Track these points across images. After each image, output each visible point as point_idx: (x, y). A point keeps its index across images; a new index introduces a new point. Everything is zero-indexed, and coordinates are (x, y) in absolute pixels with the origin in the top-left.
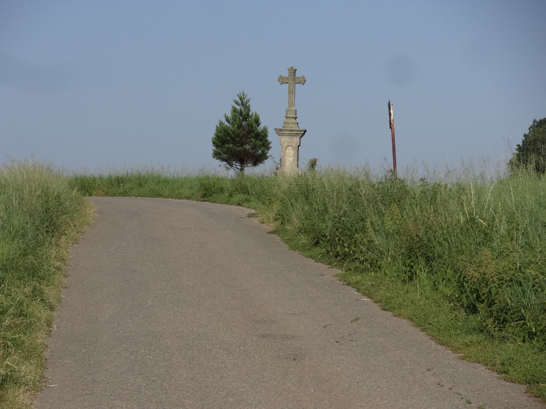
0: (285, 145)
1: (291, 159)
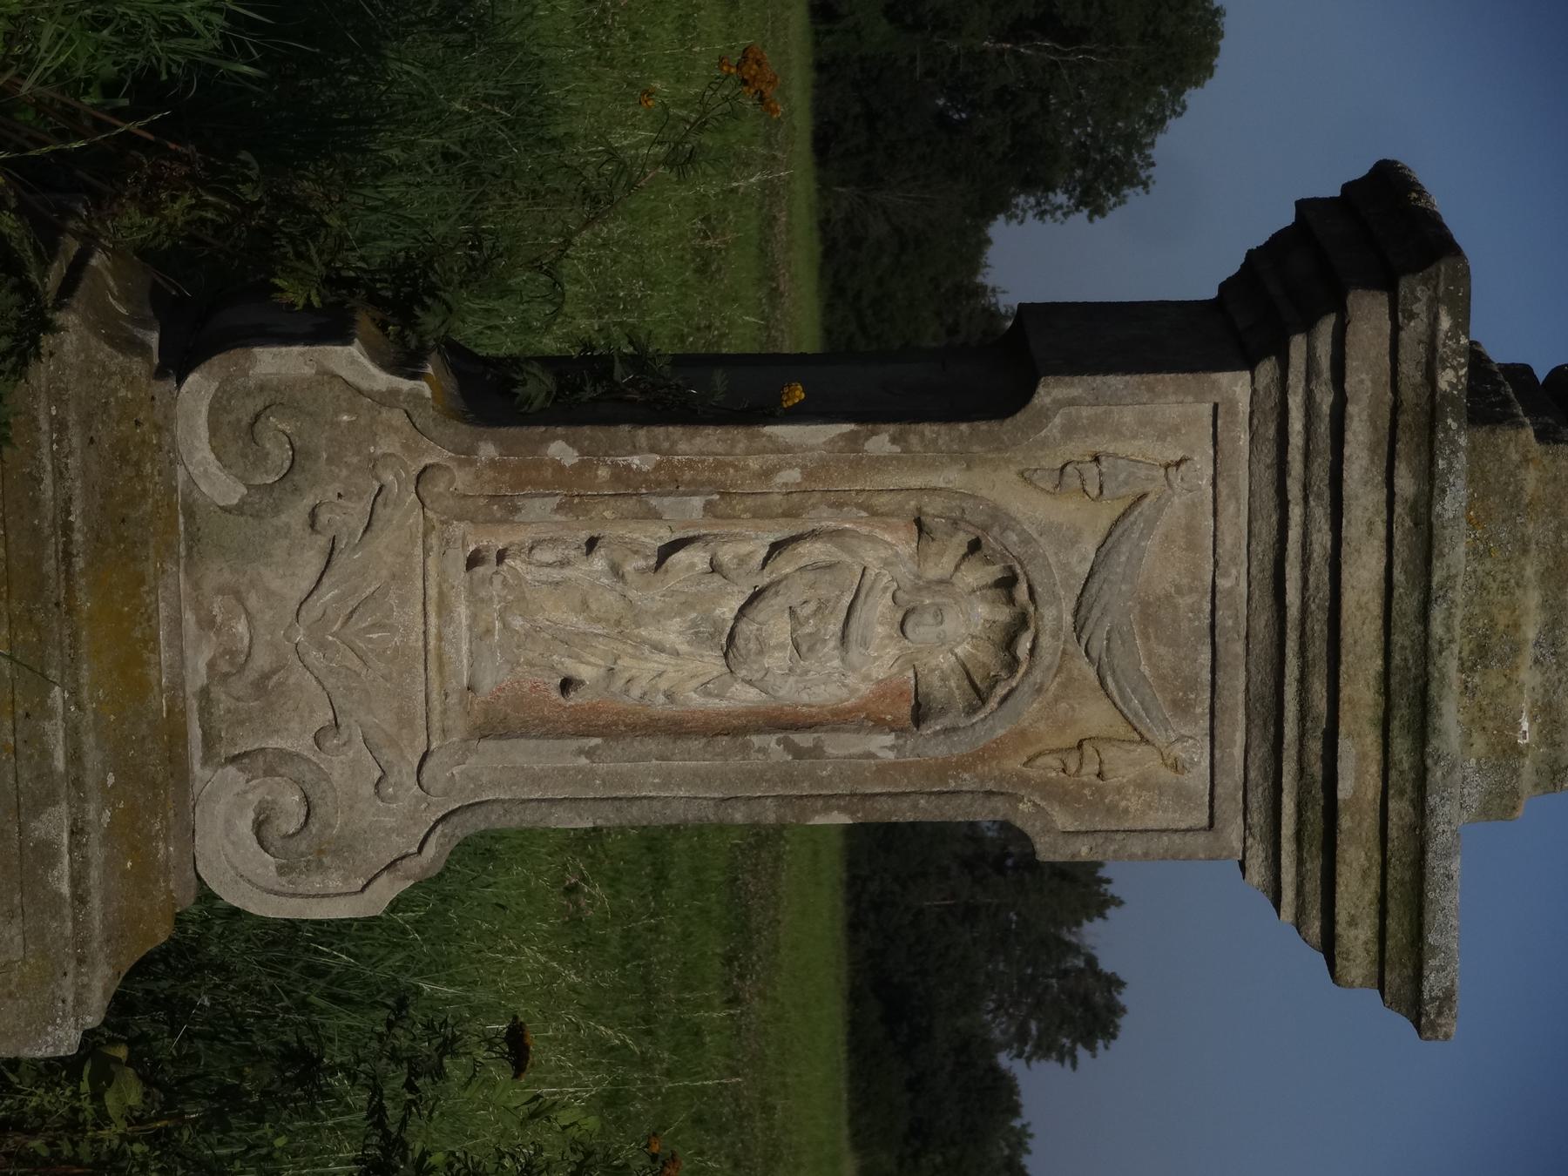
0: (1031, 508)
1: (670, 666)
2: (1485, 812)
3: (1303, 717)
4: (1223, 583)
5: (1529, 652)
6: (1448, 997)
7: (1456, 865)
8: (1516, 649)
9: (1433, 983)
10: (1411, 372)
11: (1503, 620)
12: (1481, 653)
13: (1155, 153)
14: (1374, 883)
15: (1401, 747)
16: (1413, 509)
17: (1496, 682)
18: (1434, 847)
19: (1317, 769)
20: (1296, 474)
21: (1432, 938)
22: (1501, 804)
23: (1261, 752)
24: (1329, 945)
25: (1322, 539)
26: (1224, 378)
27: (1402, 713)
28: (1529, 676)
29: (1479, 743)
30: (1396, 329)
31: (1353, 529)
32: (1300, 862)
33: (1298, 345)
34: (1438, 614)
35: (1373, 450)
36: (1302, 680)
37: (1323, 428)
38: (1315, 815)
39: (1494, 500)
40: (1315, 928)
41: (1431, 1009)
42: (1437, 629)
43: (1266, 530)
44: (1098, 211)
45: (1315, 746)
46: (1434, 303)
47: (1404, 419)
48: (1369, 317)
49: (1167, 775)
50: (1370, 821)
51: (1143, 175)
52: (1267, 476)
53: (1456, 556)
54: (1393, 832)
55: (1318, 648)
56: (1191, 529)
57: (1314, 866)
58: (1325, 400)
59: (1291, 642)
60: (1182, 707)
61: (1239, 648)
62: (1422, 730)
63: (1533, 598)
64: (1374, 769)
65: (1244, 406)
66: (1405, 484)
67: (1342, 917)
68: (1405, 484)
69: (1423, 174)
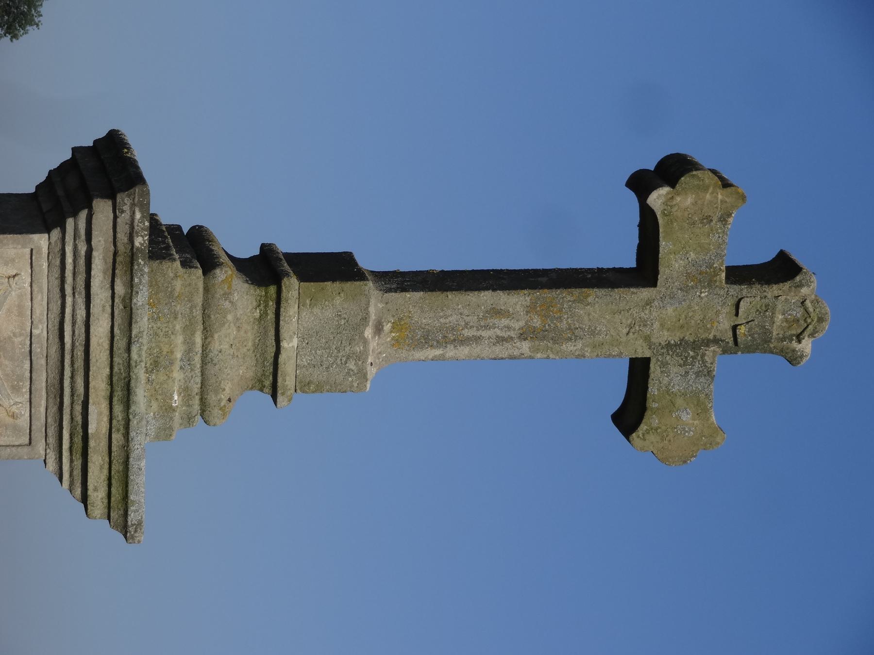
2: (157, 437)
3: (72, 395)
4: (36, 332)
5: (178, 364)
6: (139, 524)
7: (143, 464)
8: (172, 363)
9: (132, 518)
10: (122, 237)
11: (165, 350)
12: (156, 364)
13: (42, 10)
14: (106, 472)
15: (118, 409)
16: (123, 300)
17: (162, 378)
18: (133, 456)
19: (79, 419)
20: (70, 282)
21: (132, 497)
22: (165, 433)
23: (53, 410)
24: (85, 499)
25: (81, 313)
26: (36, 237)
27: (118, 394)
28: (177, 375)
29: (155, 405)
30: (115, 218)
31: (95, 309)
32: (71, 461)
33: (70, 222)
34: (134, 349)
35: (105, 273)
36: (72, 377)
37: (82, 261)
38: (78, 440)
39: (161, 295)
40: (78, 491)
41: (131, 529)
42: (134, 356)
43: (56, 308)
44: (15, 36)
45: (78, 408)
46: (133, 205)
47: (119, 259)
48: (102, 209)
49: (9, 420)
50: (104, 443)
51: (36, 20)
52: (57, 283)
53: (143, 323)
54: (114, 449)
55: (80, 363)
56: (20, 307)
57: (78, 463)
58: (83, 249)
59: (68, 358)
60: (16, 389)
61: (43, 362)
62: (127, 403)
63: (179, 339)
64: (106, 419)
65: (45, 250)
66: (120, 289)
67: (90, 486)
68: (120, 289)
69: (131, 138)
